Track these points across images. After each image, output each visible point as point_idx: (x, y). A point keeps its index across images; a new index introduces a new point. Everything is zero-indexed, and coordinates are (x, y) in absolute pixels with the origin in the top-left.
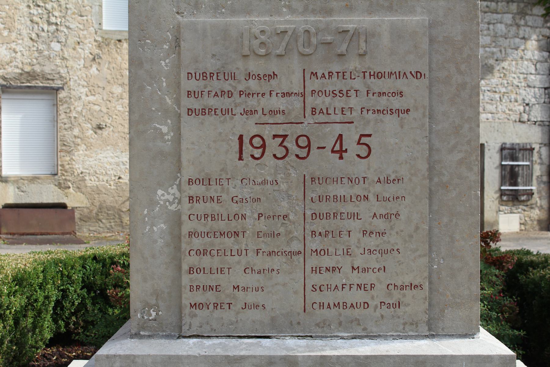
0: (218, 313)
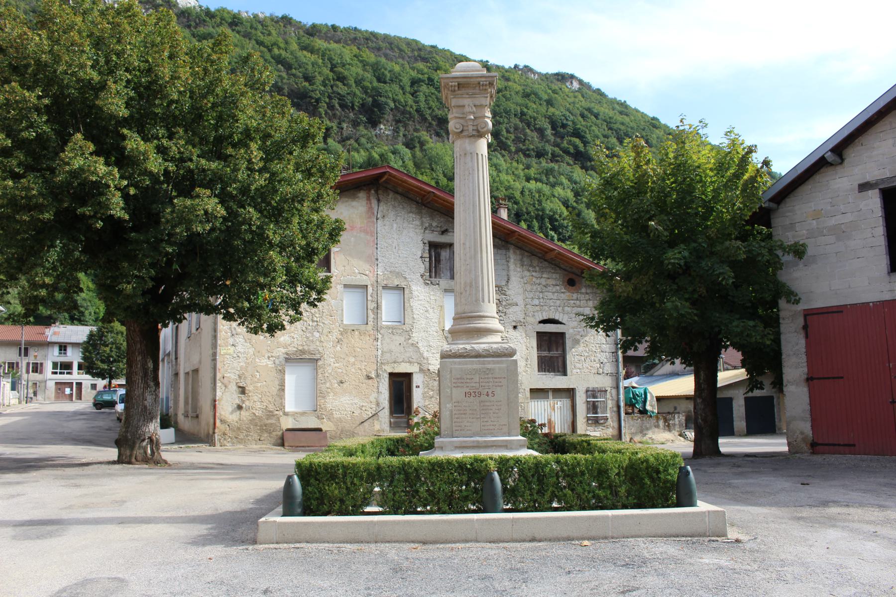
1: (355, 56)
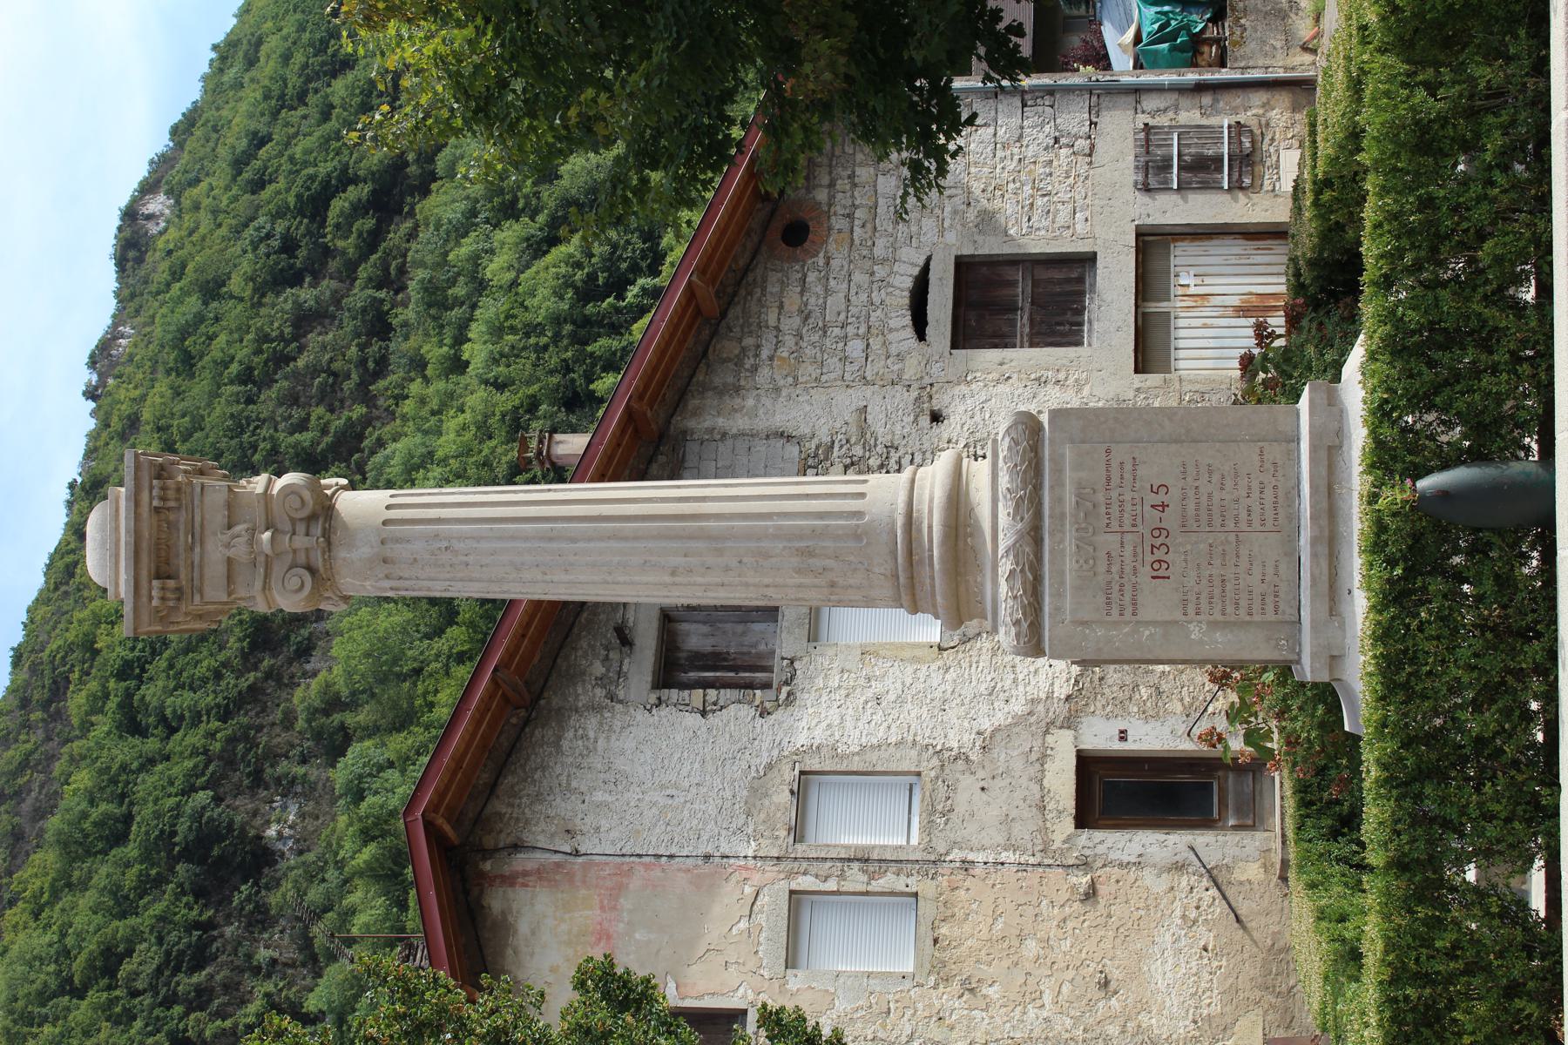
0: (1281, 594)
1: (36, 916)
